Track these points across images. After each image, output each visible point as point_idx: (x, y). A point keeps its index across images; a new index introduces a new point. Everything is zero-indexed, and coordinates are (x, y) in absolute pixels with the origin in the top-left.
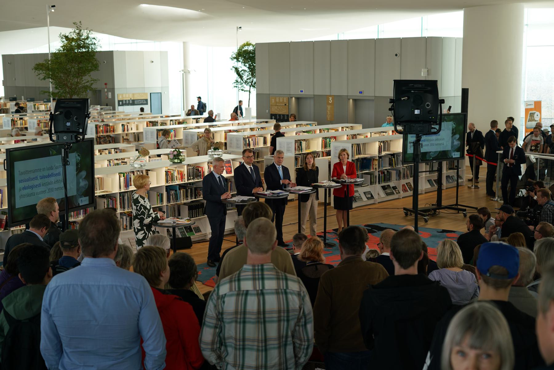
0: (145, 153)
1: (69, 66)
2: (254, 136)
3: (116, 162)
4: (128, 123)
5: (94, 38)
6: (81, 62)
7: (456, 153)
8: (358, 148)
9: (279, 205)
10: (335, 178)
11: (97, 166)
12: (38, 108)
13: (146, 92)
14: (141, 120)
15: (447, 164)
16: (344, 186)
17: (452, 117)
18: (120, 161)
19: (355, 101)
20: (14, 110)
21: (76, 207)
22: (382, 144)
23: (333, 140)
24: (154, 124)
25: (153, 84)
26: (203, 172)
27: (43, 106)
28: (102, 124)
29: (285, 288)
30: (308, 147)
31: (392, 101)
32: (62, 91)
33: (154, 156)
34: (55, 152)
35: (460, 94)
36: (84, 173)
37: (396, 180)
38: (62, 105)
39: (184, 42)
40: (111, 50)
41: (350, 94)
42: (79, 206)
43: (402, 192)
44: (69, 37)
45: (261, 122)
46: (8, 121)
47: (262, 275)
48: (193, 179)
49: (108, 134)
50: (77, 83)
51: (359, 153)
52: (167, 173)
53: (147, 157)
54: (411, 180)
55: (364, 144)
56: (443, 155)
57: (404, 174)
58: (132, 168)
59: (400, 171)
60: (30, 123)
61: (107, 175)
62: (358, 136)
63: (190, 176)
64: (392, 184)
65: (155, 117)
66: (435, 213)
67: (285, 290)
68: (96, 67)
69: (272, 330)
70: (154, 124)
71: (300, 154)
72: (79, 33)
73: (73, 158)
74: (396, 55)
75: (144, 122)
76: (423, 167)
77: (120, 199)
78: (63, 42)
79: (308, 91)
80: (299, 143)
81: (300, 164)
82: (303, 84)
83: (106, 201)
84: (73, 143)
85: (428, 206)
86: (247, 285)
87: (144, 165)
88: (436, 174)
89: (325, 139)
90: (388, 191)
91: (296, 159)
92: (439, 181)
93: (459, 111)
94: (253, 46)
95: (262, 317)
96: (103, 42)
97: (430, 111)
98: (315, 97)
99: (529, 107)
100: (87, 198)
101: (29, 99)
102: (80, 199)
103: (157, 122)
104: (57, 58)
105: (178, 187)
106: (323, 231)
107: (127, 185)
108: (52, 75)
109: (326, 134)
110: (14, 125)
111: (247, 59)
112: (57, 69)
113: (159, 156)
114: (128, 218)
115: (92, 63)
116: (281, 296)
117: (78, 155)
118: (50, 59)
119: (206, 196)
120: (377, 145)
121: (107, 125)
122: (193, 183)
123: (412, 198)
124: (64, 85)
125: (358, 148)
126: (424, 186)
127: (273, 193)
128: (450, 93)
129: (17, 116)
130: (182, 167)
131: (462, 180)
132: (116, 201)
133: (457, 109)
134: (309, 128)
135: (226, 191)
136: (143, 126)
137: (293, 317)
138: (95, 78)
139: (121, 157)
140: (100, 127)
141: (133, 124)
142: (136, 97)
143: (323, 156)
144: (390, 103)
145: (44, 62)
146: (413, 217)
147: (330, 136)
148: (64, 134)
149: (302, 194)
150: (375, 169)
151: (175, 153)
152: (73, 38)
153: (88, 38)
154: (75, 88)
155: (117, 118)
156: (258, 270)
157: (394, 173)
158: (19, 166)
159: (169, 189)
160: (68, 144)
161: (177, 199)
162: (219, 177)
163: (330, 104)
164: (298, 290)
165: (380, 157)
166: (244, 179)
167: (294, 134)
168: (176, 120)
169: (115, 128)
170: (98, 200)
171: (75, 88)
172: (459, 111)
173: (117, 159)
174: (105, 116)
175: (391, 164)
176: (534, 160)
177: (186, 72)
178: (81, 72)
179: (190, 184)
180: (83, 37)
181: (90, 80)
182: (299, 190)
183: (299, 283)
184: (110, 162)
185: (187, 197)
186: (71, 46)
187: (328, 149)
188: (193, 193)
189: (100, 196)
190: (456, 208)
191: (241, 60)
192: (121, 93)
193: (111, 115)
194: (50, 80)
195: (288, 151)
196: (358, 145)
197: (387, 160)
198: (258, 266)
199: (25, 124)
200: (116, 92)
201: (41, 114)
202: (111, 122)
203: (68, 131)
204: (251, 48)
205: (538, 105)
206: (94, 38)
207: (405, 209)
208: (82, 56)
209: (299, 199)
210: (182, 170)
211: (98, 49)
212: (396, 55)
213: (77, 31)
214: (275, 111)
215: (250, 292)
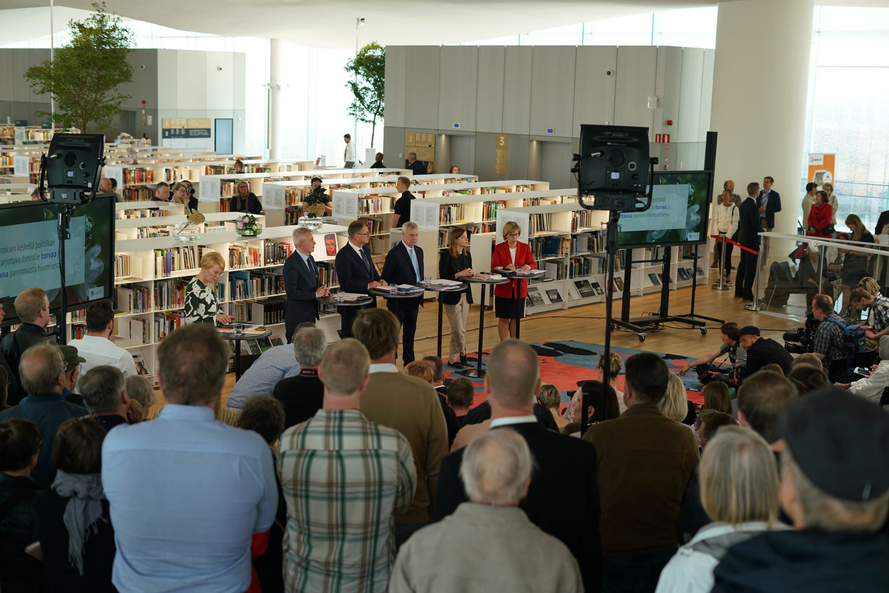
1: (83, 73)
2: (376, 195)
3: (152, 231)
4: (177, 167)
5: (123, 30)
6: (102, 67)
7: (693, 234)
8: (540, 221)
9: (407, 309)
11: (121, 236)
12: (33, 137)
13: (208, 117)
15: (680, 250)
16: (512, 280)
18: (159, 230)
19: (541, 144)
22: (578, 215)
23: (500, 206)
24: (218, 170)
25: (220, 104)
27: (42, 134)
28: (134, 167)
29: (376, 447)
30: (461, 216)
31: (576, 157)
32: (70, 113)
36: (97, 249)
37: (599, 273)
38: (62, 144)
39: (272, 40)
40: (154, 47)
42: (89, 301)
45: (389, 173)
47: (340, 427)
48: (273, 262)
49: (144, 184)
51: (541, 228)
52: (232, 251)
53: (202, 225)
55: (549, 215)
56: (672, 237)
58: (177, 242)
60: (18, 161)
62: (541, 201)
63: (268, 258)
64: (591, 279)
65: (220, 159)
66: (656, 328)
67: (376, 451)
68: (126, 76)
69: (356, 513)
70: (218, 170)
71: (447, 227)
72: (100, 21)
76: (641, 254)
77: (155, 291)
78: (75, 33)
79: (466, 126)
80: (446, 209)
81: (446, 242)
82: (459, 114)
83: (132, 293)
84: (77, 205)
85: (647, 315)
86: (315, 442)
88: (661, 265)
89: (488, 203)
90: (585, 290)
91: (441, 235)
92: (665, 277)
93: (700, 166)
94: (383, 50)
95: (337, 492)
96: (139, 34)
97: (636, 175)
98: (477, 135)
99: (815, 163)
102: (91, 290)
103: (223, 168)
105: (249, 274)
107: (167, 269)
108: (54, 86)
111: (372, 70)
113: (222, 223)
114: (167, 322)
115: (121, 69)
117: (90, 221)
118: (52, 60)
119: (292, 291)
120: (570, 216)
121: (142, 170)
122: (273, 269)
123: (621, 302)
127: (399, 289)
130: (257, 243)
132: (149, 294)
133: (697, 164)
134: (464, 185)
135: (319, 285)
136: (200, 173)
137: (388, 492)
138: (124, 94)
139: (160, 224)
140: (130, 172)
141: (183, 169)
142: (193, 125)
143: (484, 231)
144: (574, 160)
145: (43, 66)
147: (497, 200)
148: (62, 190)
149: (444, 293)
150: (565, 254)
151: (247, 220)
152: (91, 29)
153: (114, 29)
154: (93, 109)
156: (335, 418)
157: (595, 262)
159: (233, 276)
160: (69, 206)
161: (246, 294)
162: (308, 260)
164: (395, 449)
165: (574, 236)
166: (349, 268)
167: (441, 195)
168: (253, 165)
169: (155, 176)
170: (120, 292)
172: (700, 166)
173: (154, 227)
175: (590, 248)
176: (816, 250)
177: (273, 88)
178: (103, 84)
179: (268, 269)
180: (107, 28)
181: (116, 96)
182: (441, 286)
183: (398, 437)
184: (142, 231)
185: (263, 290)
186: (88, 41)
187: (492, 220)
188: (273, 284)
189: (123, 286)
190: (691, 320)
191: (362, 72)
192: (167, 118)
194: (52, 95)
195: (429, 220)
196: (540, 216)
197: (585, 241)
198: (335, 413)
199: (10, 164)
201: (36, 147)
202: (149, 165)
203: (68, 185)
204: (378, 53)
205: (829, 161)
206: (123, 30)
209: (439, 300)
210: (256, 247)
211: (132, 46)
212: (609, 73)
213: (98, 18)
215: (318, 453)
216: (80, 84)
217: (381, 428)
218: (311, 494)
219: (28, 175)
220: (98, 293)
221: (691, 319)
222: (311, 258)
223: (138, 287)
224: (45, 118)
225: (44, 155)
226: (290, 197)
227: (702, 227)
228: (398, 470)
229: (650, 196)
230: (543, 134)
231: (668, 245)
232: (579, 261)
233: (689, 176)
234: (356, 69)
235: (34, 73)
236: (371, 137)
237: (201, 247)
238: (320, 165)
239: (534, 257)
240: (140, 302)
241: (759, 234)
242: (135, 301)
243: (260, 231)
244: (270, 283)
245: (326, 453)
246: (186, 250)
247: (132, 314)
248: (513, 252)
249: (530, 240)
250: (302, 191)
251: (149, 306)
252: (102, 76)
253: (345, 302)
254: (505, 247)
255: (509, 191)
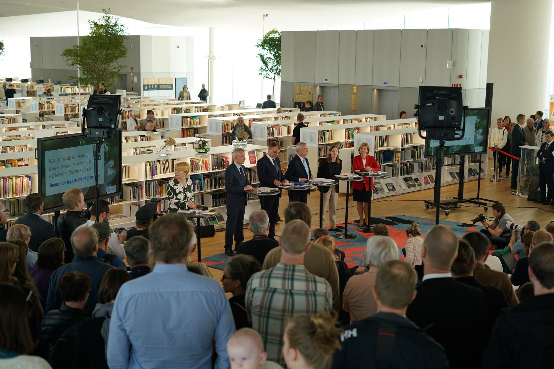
0: (170, 142)
1: (97, 53)
2: (278, 125)
6: (109, 49)
7: (479, 147)
8: (382, 140)
9: (299, 196)
10: (358, 171)
11: (124, 154)
13: (171, 77)
14: (167, 106)
15: (469, 157)
17: (476, 111)
18: (146, 149)
19: (379, 91)
20: (42, 93)
21: (104, 195)
22: (405, 136)
23: (356, 131)
26: (228, 162)
27: (70, 89)
29: (314, 290)
30: (331, 138)
32: (89, 77)
33: (179, 145)
34: (84, 142)
35: (485, 86)
36: (112, 163)
37: (419, 172)
38: (95, 101)
41: (374, 84)
42: (107, 195)
43: (423, 185)
44: (98, 23)
46: (36, 104)
47: (293, 275)
48: (217, 168)
50: (105, 69)
51: (382, 145)
53: (173, 146)
54: (433, 173)
55: (387, 137)
56: (466, 149)
57: (426, 167)
59: (422, 163)
60: (57, 107)
61: (134, 163)
62: (381, 127)
64: (414, 176)
65: (180, 104)
66: (456, 207)
67: (314, 292)
68: (123, 54)
71: (323, 145)
73: (104, 148)
74: (422, 46)
75: (169, 108)
77: (146, 187)
80: (322, 133)
81: (322, 154)
82: (328, 73)
83: (132, 189)
86: (276, 283)
87: (170, 155)
90: (410, 183)
91: (319, 149)
92: (461, 174)
93: (483, 105)
96: (129, 26)
97: (454, 117)
98: (339, 86)
100: (115, 186)
101: (56, 82)
102: (108, 188)
103: (181, 109)
104: (85, 45)
106: (344, 222)
107: (153, 174)
108: (80, 61)
109: (349, 125)
110: (42, 108)
111: (273, 46)
112: (86, 55)
113: (184, 144)
116: (310, 298)
117: (107, 145)
118: (78, 45)
119: (229, 185)
120: (400, 137)
122: (217, 173)
123: (433, 190)
124: (92, 71)
125: (382, 140)
126: (446, 178)
128: (475, 99)
129: (44, 99)
130: (207, 157)
131: (484, 174)
132: (142, 189)
134: (332, 118)
141: (158, 111)
142: (161, 82)
144: (416, 108)
146: (434, 209)
147: (353, 127)
150: (397, 161)
151: (201, 143)
152: (102, 25)
153: (116, 25)
154: (103, 74)
155: (143, 103)
156: (290, 270)
158: (49, 155)
161: (201, 188)
162: (240, 168)
163: (354, 94)
165: (403, 150)
166: (266, 170)
168: (201, 107)
170: (124, 187)
171: (103, 74)
172: (483, 105)
174: (131, 101)
175: (413, 157)
177: (211, 58)
178: (110, 59)
179: (214, 173)
180: (111, 24)
182: (322, 182)
183: (326, 284)
184: (136, 150)
185: (211, 186)
187: (351, 140)
188: (217, 182)
189: (126, 184)
190: (477, 201)
192: (146, 78)
193: (136, 100)
194: (79, 66)
196: (381, 137)
197: (410, 152)
198: (290, 266)
200: (142, 76)
203: (99, 126)
204: (276, 36)
207: (426, 202)
208: (110, 43)
210: (207, 159)
211: (127, 34)
213: (106, 18)
214: (300, 99)
215: (278, 290)
216: (96, 59)
217: (317, 278)
218: (271, 315)
219: (63, 115)
220: (112, 189)
221: (477, 201)
222: (243, 166)
223: (135, 185)
224: (74, 80)
225: (84, 108)
226: (225, 126)
227: (484, 143)
228: (326, 304)
229: (463, 130)
230: (381, 85)
231: (463, 155)
232: (406, 165)
233: (476, 111)
234: (263, 46)
235: (68, 53)
236: (272, 87)
237: (173, 160)
238: (241, 106)
239: (378, 163)
240: (136, 194)
241: (520, 147)
242: (134, 193)
243: (209, 150)
244: (215, 181)
245: (284, 291)
246: (164, 162)
247: (132, 202)
248: (364, 161)
249: (375, 152)
250: (232, 123)
251: (142, 197)
252: (109, 54)
253: (263, 193)
254: (359, 158)
255: (361, 121)
